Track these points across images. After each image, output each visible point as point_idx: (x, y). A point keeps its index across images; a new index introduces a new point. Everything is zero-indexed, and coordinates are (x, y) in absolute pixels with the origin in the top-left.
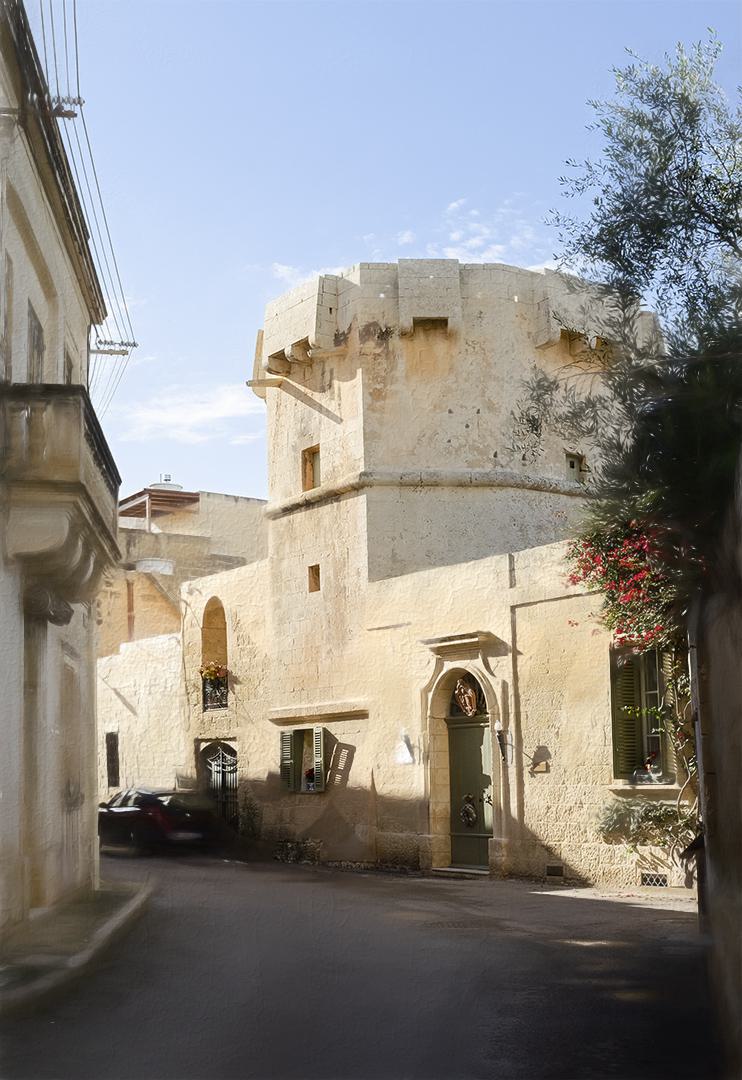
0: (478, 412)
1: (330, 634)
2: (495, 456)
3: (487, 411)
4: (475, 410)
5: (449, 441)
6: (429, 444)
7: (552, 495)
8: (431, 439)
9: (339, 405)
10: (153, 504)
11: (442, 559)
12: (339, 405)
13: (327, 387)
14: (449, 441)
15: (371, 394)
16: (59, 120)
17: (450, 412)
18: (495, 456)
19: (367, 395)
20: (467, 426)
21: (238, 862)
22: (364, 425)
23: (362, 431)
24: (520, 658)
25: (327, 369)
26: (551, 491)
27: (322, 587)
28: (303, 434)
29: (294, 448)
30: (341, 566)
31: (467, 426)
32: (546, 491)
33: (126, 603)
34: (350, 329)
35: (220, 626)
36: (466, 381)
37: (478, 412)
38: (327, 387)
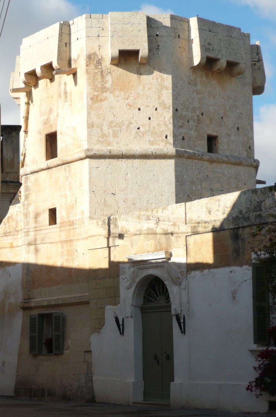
0: (156, 109)
1: (63, 252)
2: (166, 137)
3: (162, 109)
4: (155, 108)
5: (139, 128)
7: (199, 161)
8: (128, 126)
9: (71, 105)
10: (59, 324)
12: (71, 105)
13: (5, 235)
14: (139, 128)
15: (91, 99)
17: (139, 109)
18: (166, 137)
19: (89, 99)
20: (150, 119)
22: (88, 118)
23: (86, 122)
24: (2, 237)
25: (63, 82)
26: (199, 159)
27: (58, 221)
30: (71, 208)
31: (150, 119)
32: (196, 159)
34: (79, 56)
35: (18, 138)
36: (149, 89)
37: (156, 109)
38: (5, 235)
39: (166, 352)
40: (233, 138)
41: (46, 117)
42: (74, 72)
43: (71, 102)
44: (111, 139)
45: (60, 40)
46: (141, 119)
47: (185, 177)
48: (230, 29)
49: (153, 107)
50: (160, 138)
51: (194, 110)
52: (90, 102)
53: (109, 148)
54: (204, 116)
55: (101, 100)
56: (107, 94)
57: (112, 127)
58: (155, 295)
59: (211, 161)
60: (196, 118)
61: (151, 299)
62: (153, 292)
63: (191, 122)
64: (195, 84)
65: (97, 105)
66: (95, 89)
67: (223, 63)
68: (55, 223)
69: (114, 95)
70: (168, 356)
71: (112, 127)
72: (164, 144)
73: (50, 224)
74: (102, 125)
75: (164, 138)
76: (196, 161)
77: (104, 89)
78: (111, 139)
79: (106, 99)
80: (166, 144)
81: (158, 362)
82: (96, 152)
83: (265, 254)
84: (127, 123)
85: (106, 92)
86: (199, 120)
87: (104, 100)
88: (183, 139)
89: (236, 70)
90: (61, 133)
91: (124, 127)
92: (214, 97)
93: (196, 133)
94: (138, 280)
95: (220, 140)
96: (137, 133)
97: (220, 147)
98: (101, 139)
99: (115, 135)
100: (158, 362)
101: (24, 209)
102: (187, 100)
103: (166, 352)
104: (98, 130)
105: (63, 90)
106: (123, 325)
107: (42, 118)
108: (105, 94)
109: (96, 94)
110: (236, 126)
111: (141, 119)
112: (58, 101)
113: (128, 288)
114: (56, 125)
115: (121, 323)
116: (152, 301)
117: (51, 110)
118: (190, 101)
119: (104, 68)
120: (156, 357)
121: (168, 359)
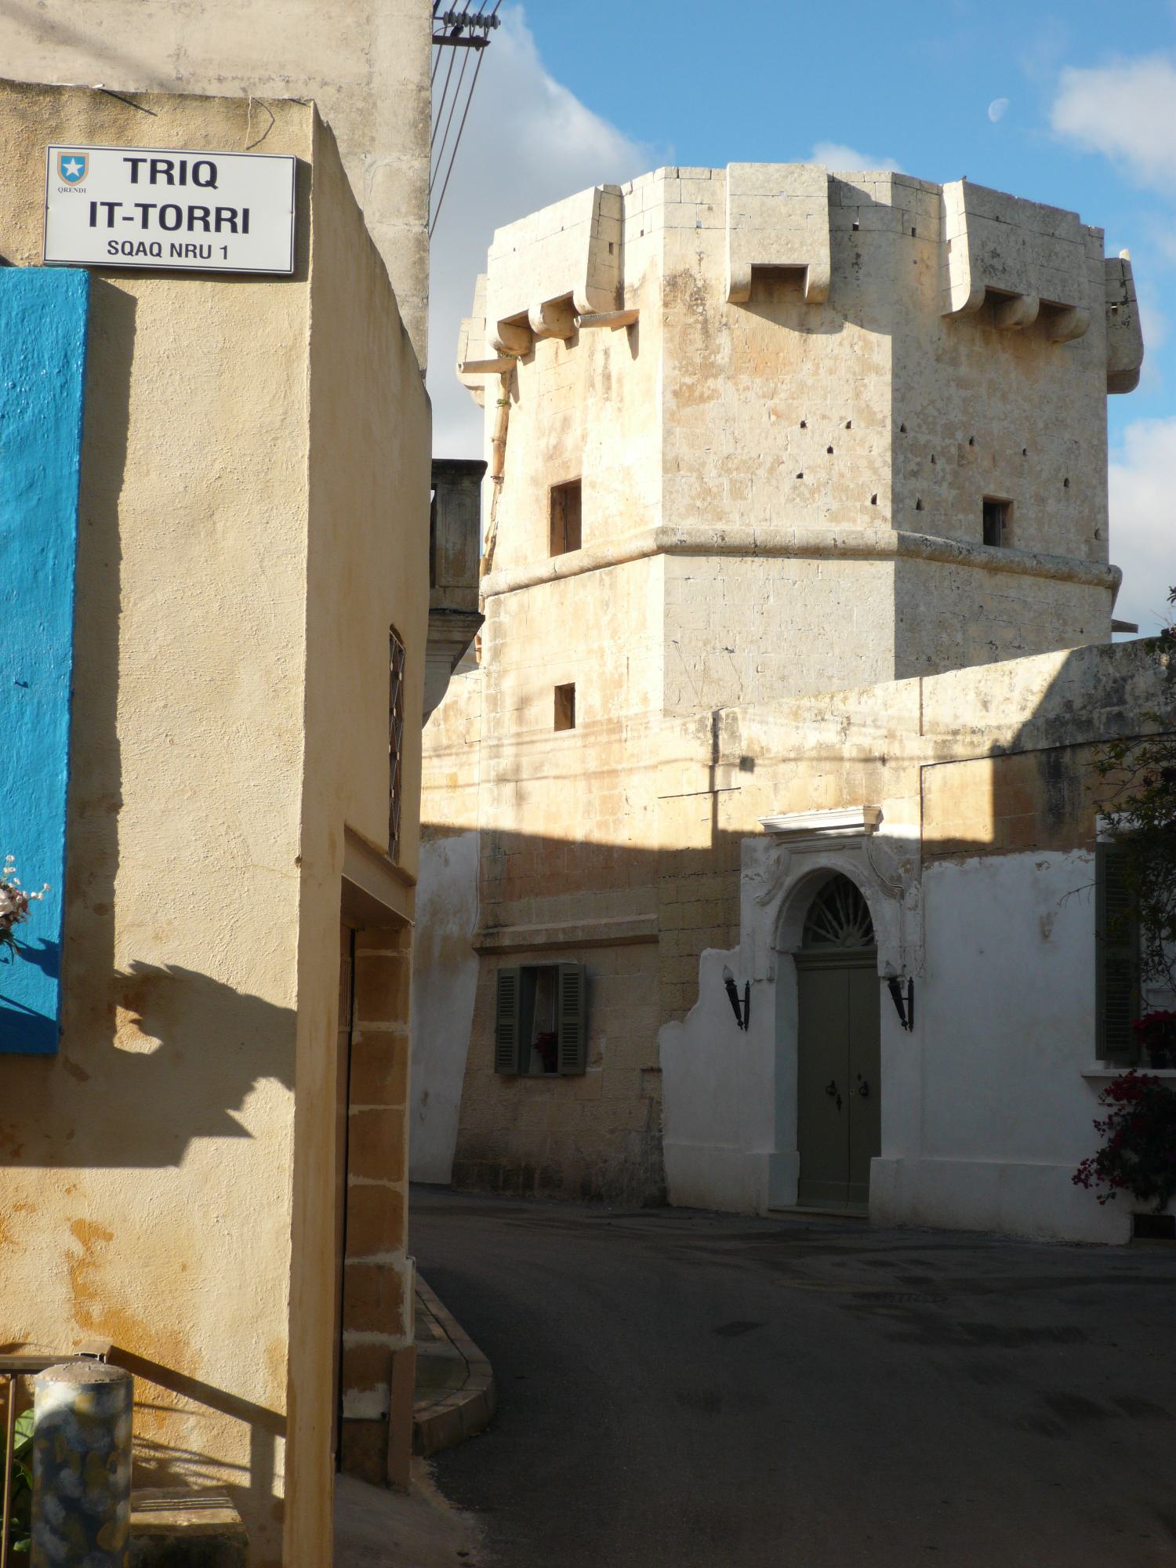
0: (848, 426)
1: (590, 803)
2: (874, 501)
3: (863, 425)
4: (845, 423)
5: (800, 476)
6: (768, 481)
7: (960, 568)
8: (772, 470)
11: (903, 429)
12: (620, 410)
14: (800, 476)
15: (676, 394)
16: (268, 1391)
17: (803, 425)
18: (874, 501)
19: (669, 396)
20: (830, 450)
21: (76, 459)
22: (665, 447)
25: (600, 347)
27: (579, 718)
28: (553, 455)
29: (535, 481)
30: (614, 685)
31: (830, 450)
33: (200, 1377)
34: (644, 279)
36: (831, 372)
37: (848, 426)
39: (859, 1077)
40: (1051, 506)
41: (553, 441)
42: (631, 321)
43: (621, 401)
44: (726, 502)
45: (595, 236)
46: (808, 452)
47: (922, 608)
48: (1050, 215)
49: (841, 418)
50: (858, 504)
51: (949, 430)
52: (673, 403)
53: (720, 526)
54: (977, 448)
55: (702, 399)
56: (717, 383)
57: (729, 471)
58: (835, 924)
59: (993, 568)
60: (954, 451)
61: (823, 932)
62: (830, 916)
63: (941, 463)
64: (954, 362)
65: (688, 411)
66: (686, 367)
67: (1029, 307)
68: (572, 725)
69: (736, 384)
70: (866, 1086)
71: (729, 471)
72: (867, 518)
73: (559, 726)
74: (704, 464)
75: (868, 502)
76: (953, 567)
77: (709, 369)
78: (726, 502)
79: (714, 395)
80: (873, 519)
81: (839, 1102)
82: (684, 537)
83: (1130, 821)
84: (769, 460)
85: (715, 376)
86: (961, 457)
87: (710, 398)
88: (919, 507)
89: (1066, 325)
90: (593, 485)
91: (762, 473)
92: (1004, 398)
93: (954, 492)
94: (789, 881)
95: (1017, 512)
96: (795, 488)
97: (1018, 531)
98: (698, 503)
99: (737, 493)
100: (839, 1102)
101: (488, 687)
102: (932, 402)
103: (859, 1077)
104: (693, 479)
105: (600, 370)
106: (747, 1001)
107: (543, 443)
108: (711, 382)
109: (688, 380)
110: (1062, 476)
111: (808, 452)
112: (585, 399)
113: (763, 904)
114: (580, 462)
115: (741, 996)
116: (826, 940)
117: (566, 423)
118: (939, 404)
119: (710, 313)
120: (832, 1090)
121: (865, 1095)
